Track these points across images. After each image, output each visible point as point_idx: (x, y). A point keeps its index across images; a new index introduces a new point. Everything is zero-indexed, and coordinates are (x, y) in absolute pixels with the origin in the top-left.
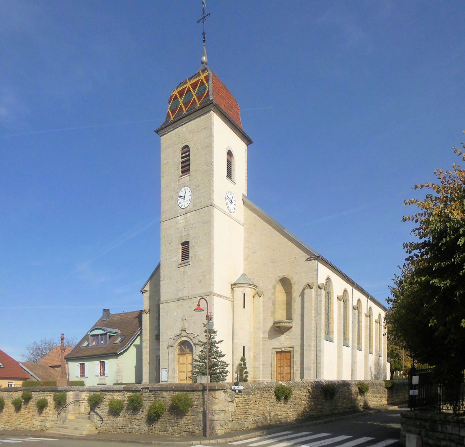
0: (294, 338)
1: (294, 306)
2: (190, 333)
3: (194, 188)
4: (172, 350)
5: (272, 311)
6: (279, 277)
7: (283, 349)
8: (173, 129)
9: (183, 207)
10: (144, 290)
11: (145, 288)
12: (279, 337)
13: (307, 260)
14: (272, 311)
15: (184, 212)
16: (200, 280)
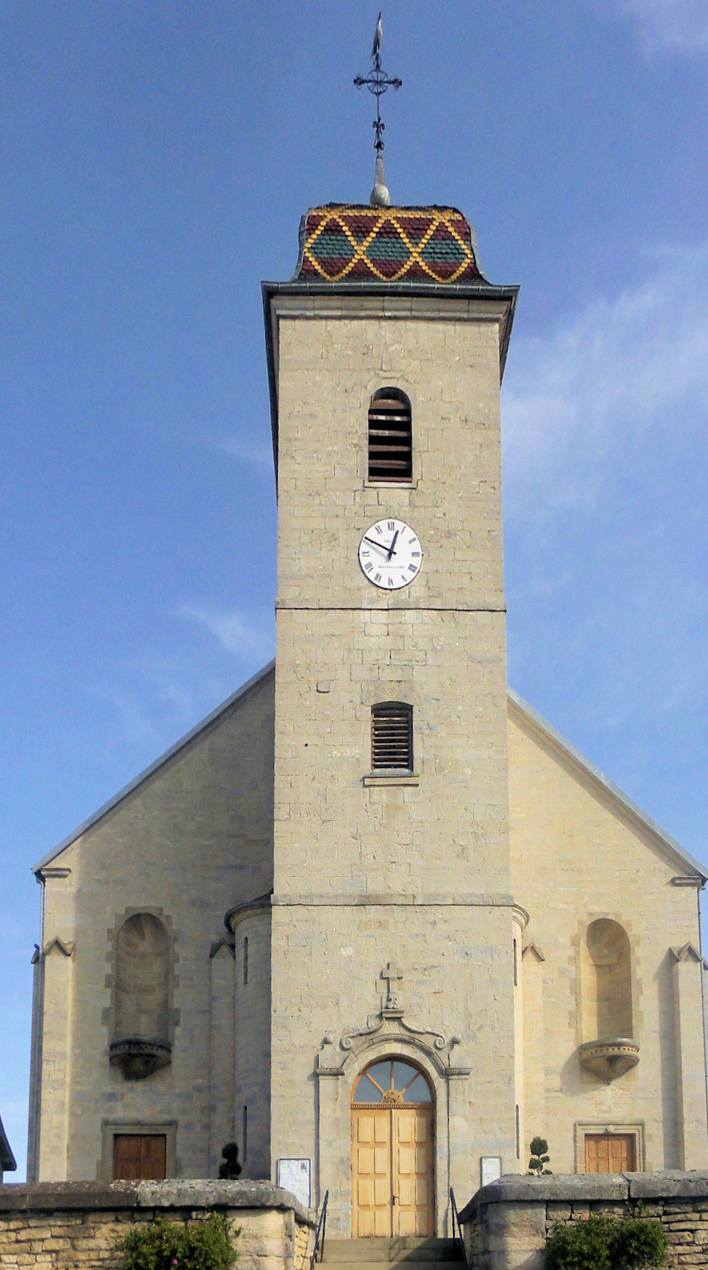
0: (641, 1098)
1: (638, 1006)
2: (421, 1030)
3: (431, 536)
4: (337, 1088)
5: (570, 1012)
6: (591, 914)
7: (612, 1129)
8: (339, 313)
9: (384, 583)
10: (47, 867)
11: (53, 862)
12: (595, 1092)
13: (673, 882)
14: (570, 1012)
15: (391, 601)
16: (463, 849)
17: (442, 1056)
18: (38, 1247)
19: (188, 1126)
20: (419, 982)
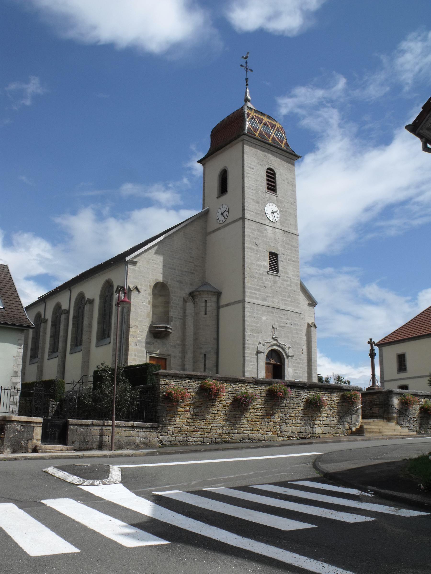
17: (287, 351)
18: (326, 395)
19: (175, 357)
20: (281, 330)
